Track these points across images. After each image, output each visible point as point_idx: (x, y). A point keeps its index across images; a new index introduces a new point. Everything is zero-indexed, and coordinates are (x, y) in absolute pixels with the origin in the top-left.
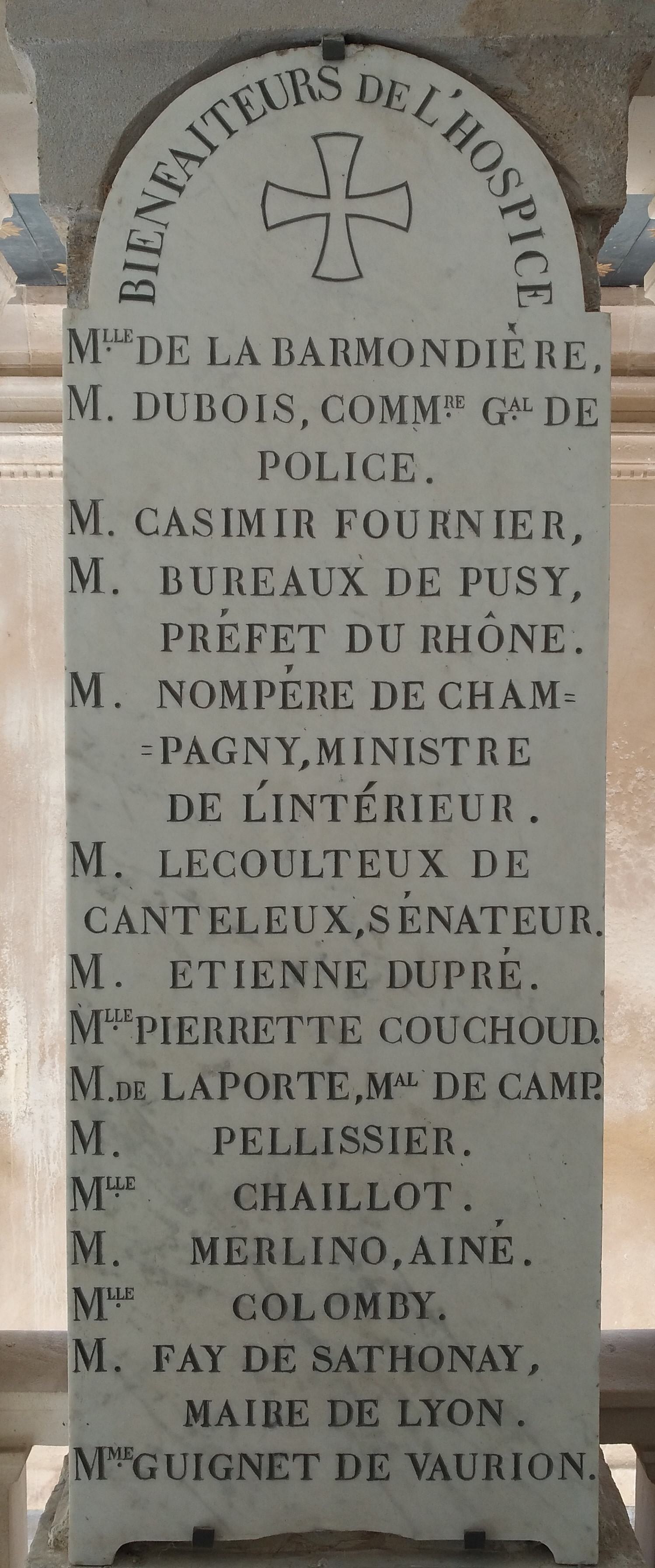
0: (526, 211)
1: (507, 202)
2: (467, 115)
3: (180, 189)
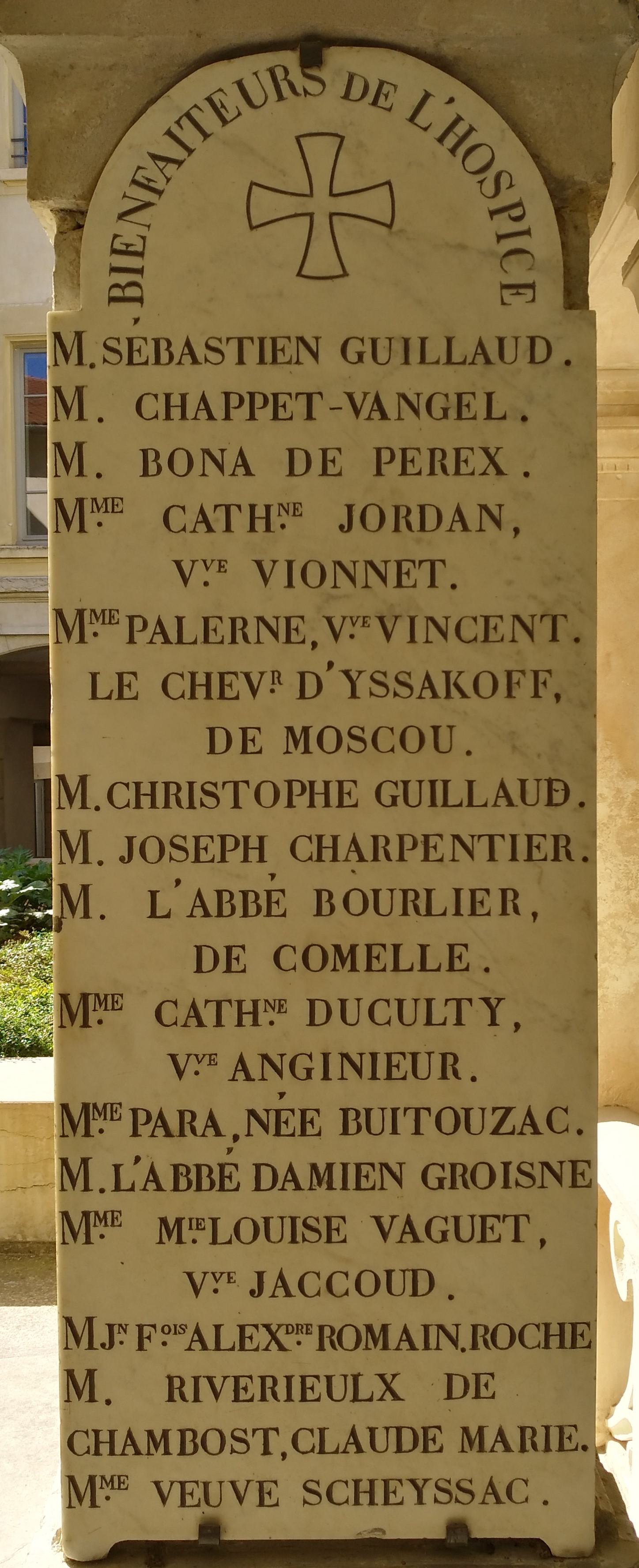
0: (516, 212)
1: (496, 204)
2: (459, 119)
3: (160, 193)
